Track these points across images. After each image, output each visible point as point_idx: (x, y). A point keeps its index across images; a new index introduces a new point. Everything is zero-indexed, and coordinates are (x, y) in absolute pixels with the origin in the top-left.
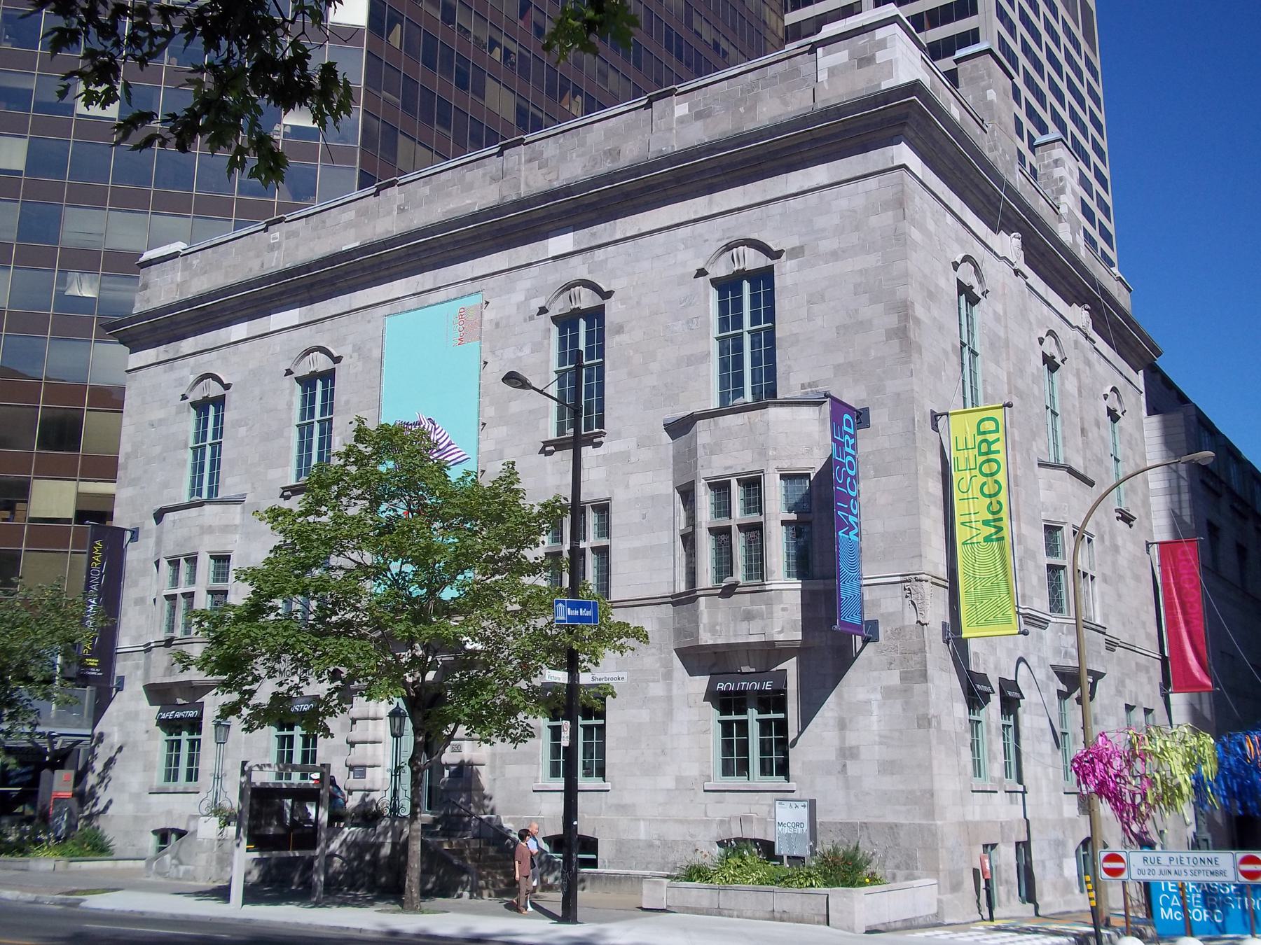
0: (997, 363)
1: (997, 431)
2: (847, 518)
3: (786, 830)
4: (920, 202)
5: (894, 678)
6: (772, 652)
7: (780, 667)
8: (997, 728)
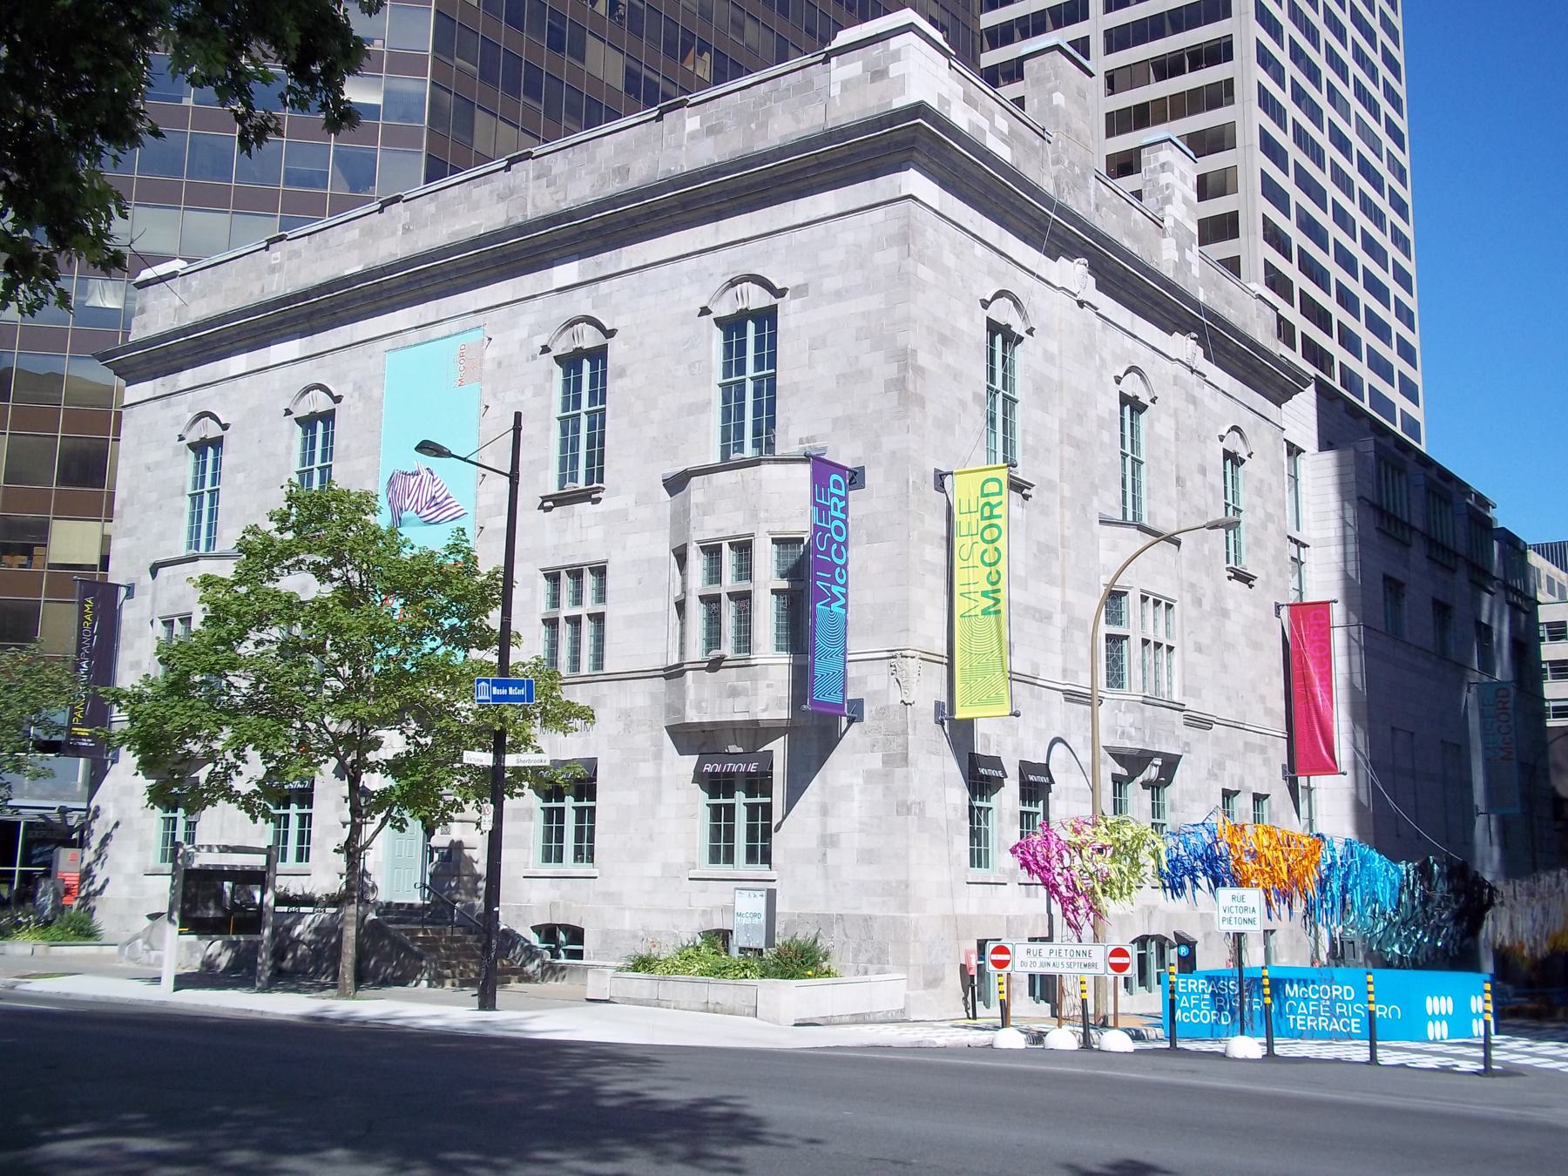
0: (1045, 409)
1: (1000, 493)
2: (829, 589)
3: (744, 921)
4: (936, 235)
5: (875, 761)
6: (757, 732)
7: (767, 748)
8: (1012, 815)
